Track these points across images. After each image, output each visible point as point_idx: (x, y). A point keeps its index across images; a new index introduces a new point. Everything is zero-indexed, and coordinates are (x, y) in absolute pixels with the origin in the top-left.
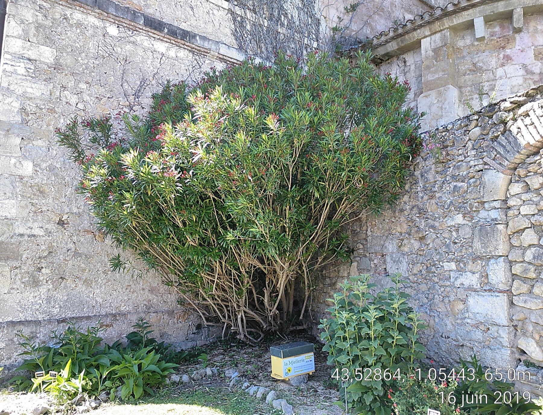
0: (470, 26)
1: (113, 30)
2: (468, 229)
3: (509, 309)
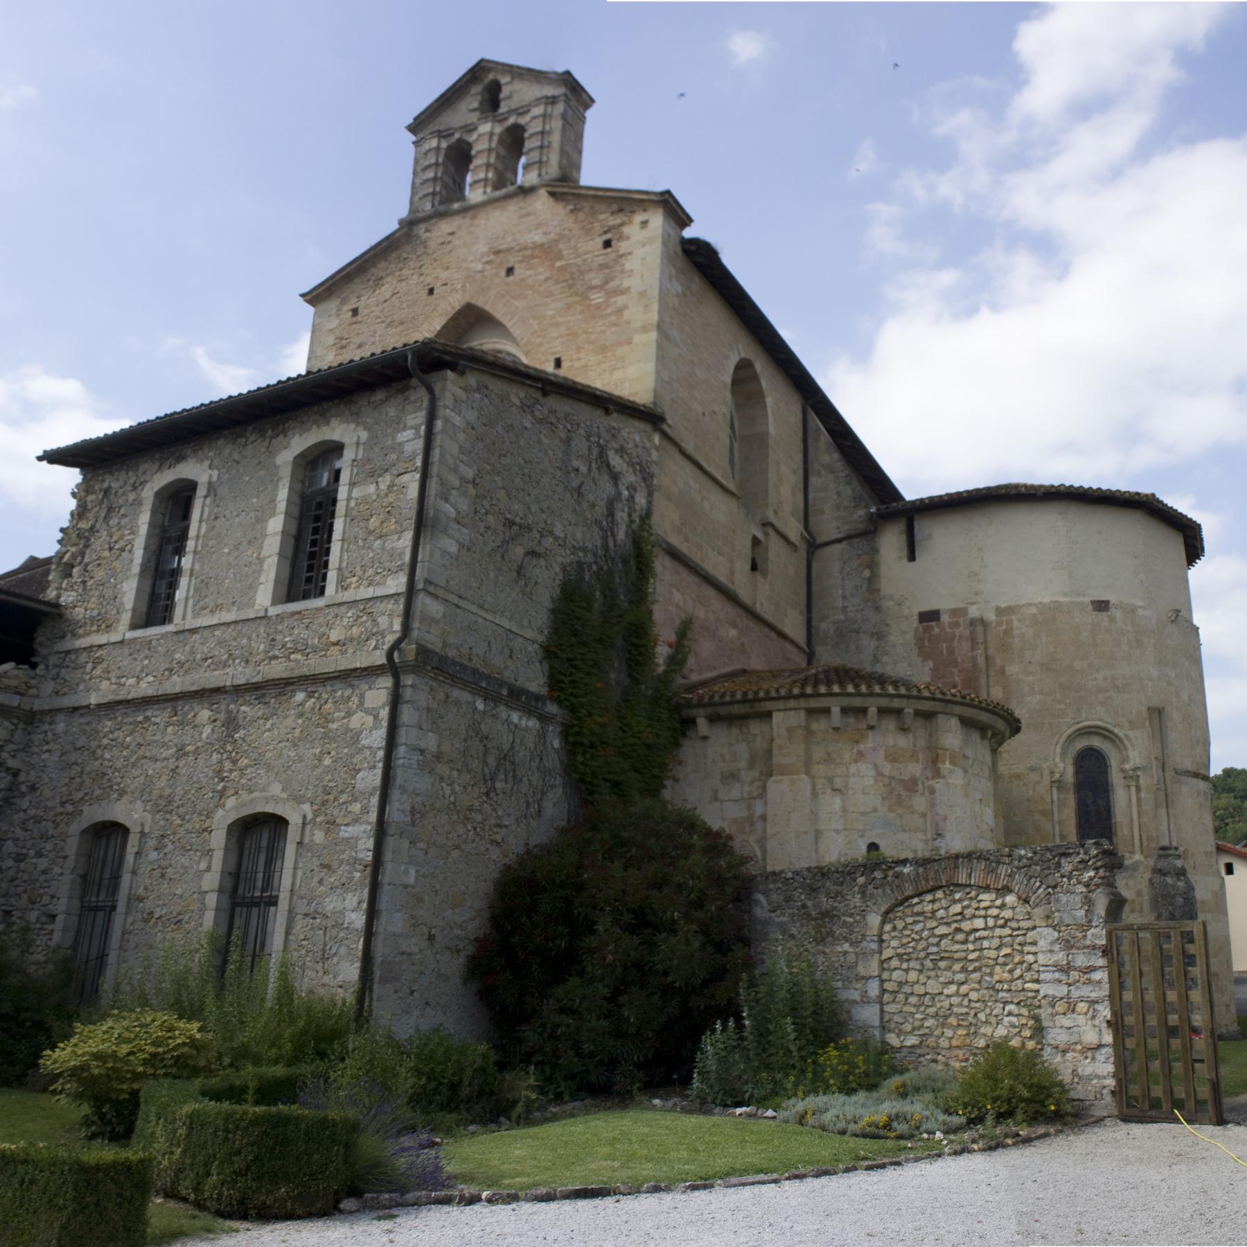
0: (827, 711)
1: (480, 705)
2: (853, 956)
3: (1099, 1121)
